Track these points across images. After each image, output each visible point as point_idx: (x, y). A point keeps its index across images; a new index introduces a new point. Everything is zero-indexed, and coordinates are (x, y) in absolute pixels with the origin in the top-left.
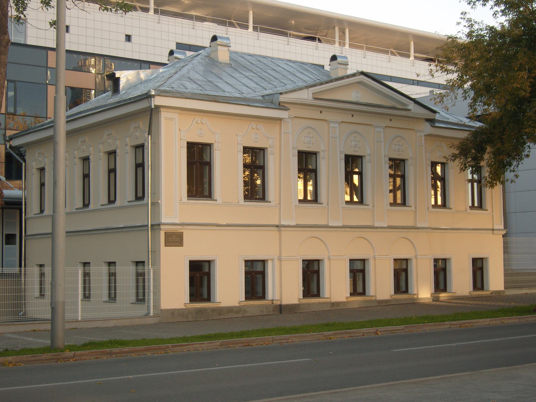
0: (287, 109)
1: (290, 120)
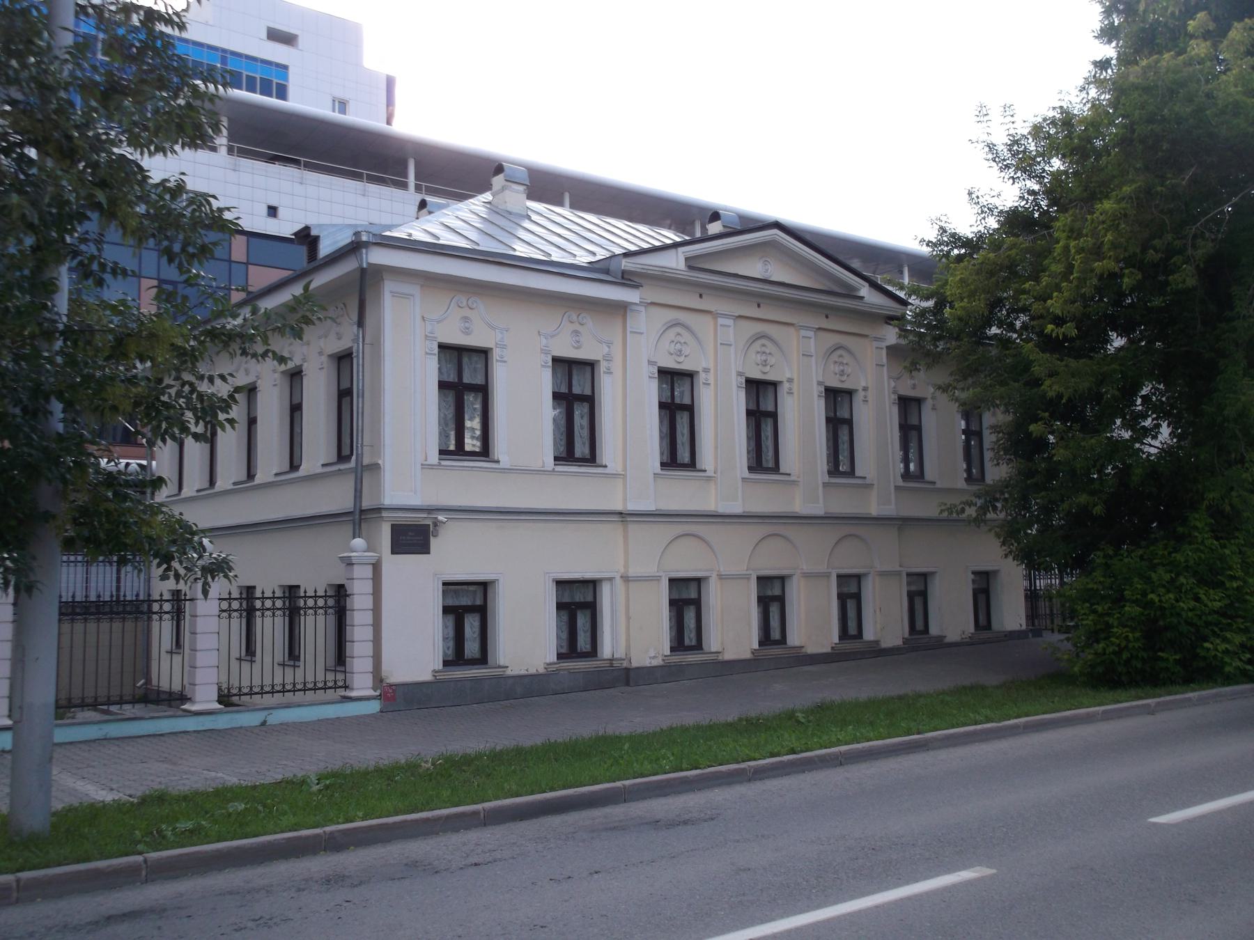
0: (636, 286)
1: (642, 309)
